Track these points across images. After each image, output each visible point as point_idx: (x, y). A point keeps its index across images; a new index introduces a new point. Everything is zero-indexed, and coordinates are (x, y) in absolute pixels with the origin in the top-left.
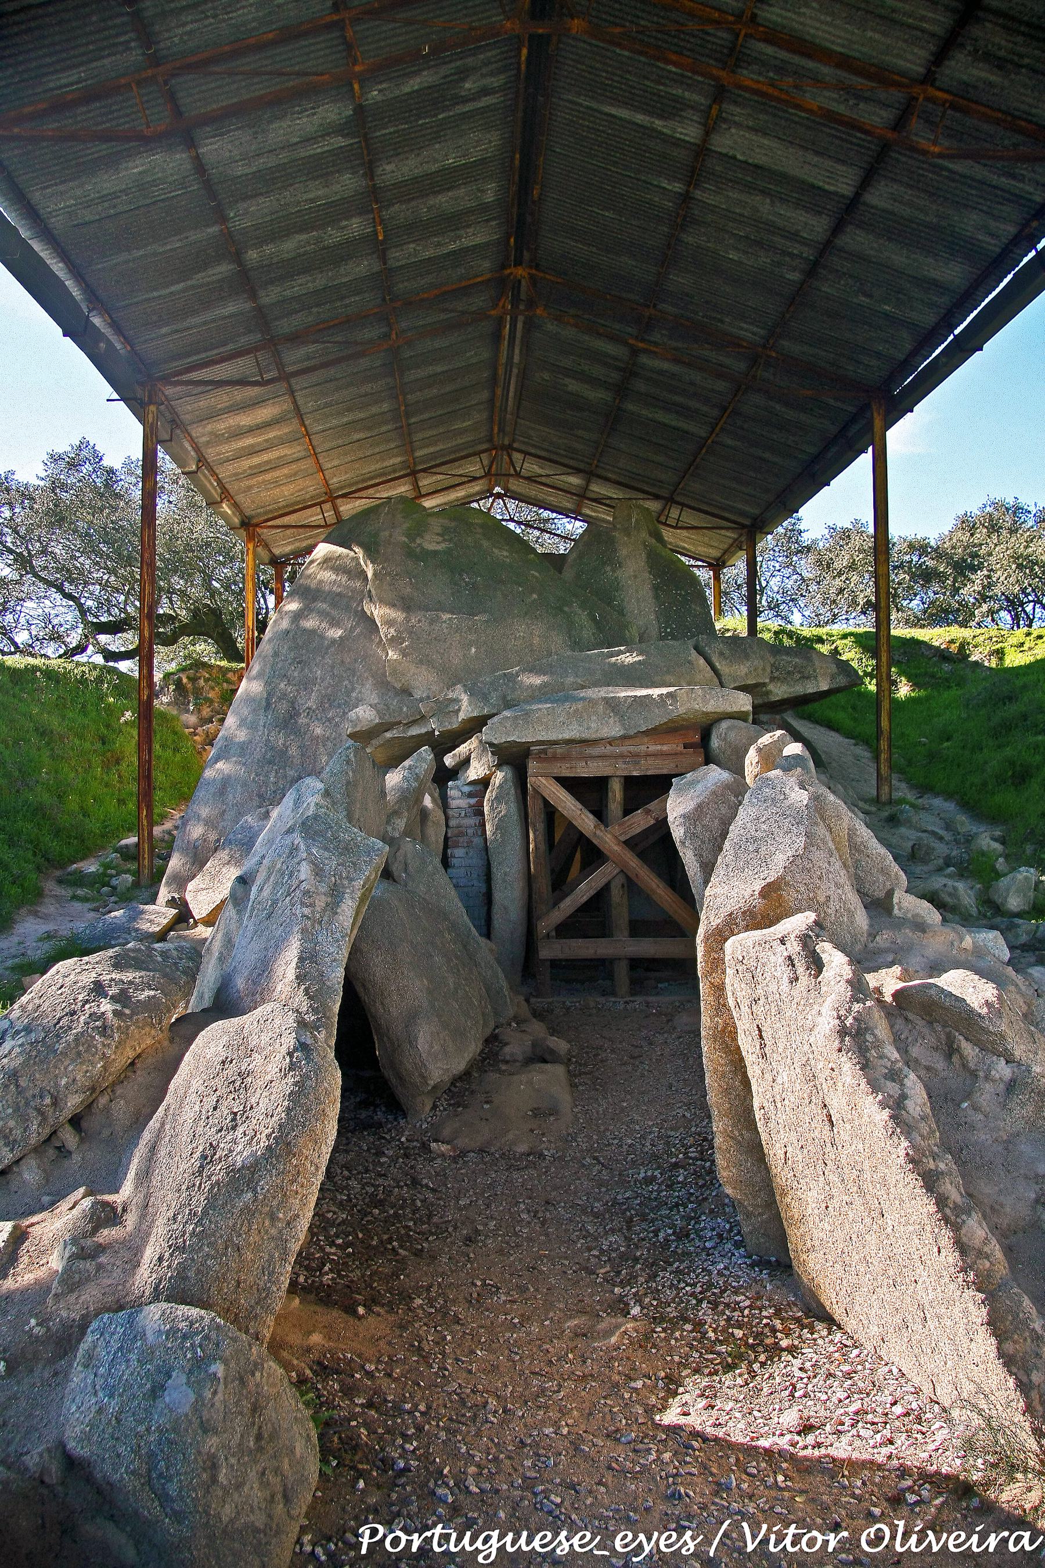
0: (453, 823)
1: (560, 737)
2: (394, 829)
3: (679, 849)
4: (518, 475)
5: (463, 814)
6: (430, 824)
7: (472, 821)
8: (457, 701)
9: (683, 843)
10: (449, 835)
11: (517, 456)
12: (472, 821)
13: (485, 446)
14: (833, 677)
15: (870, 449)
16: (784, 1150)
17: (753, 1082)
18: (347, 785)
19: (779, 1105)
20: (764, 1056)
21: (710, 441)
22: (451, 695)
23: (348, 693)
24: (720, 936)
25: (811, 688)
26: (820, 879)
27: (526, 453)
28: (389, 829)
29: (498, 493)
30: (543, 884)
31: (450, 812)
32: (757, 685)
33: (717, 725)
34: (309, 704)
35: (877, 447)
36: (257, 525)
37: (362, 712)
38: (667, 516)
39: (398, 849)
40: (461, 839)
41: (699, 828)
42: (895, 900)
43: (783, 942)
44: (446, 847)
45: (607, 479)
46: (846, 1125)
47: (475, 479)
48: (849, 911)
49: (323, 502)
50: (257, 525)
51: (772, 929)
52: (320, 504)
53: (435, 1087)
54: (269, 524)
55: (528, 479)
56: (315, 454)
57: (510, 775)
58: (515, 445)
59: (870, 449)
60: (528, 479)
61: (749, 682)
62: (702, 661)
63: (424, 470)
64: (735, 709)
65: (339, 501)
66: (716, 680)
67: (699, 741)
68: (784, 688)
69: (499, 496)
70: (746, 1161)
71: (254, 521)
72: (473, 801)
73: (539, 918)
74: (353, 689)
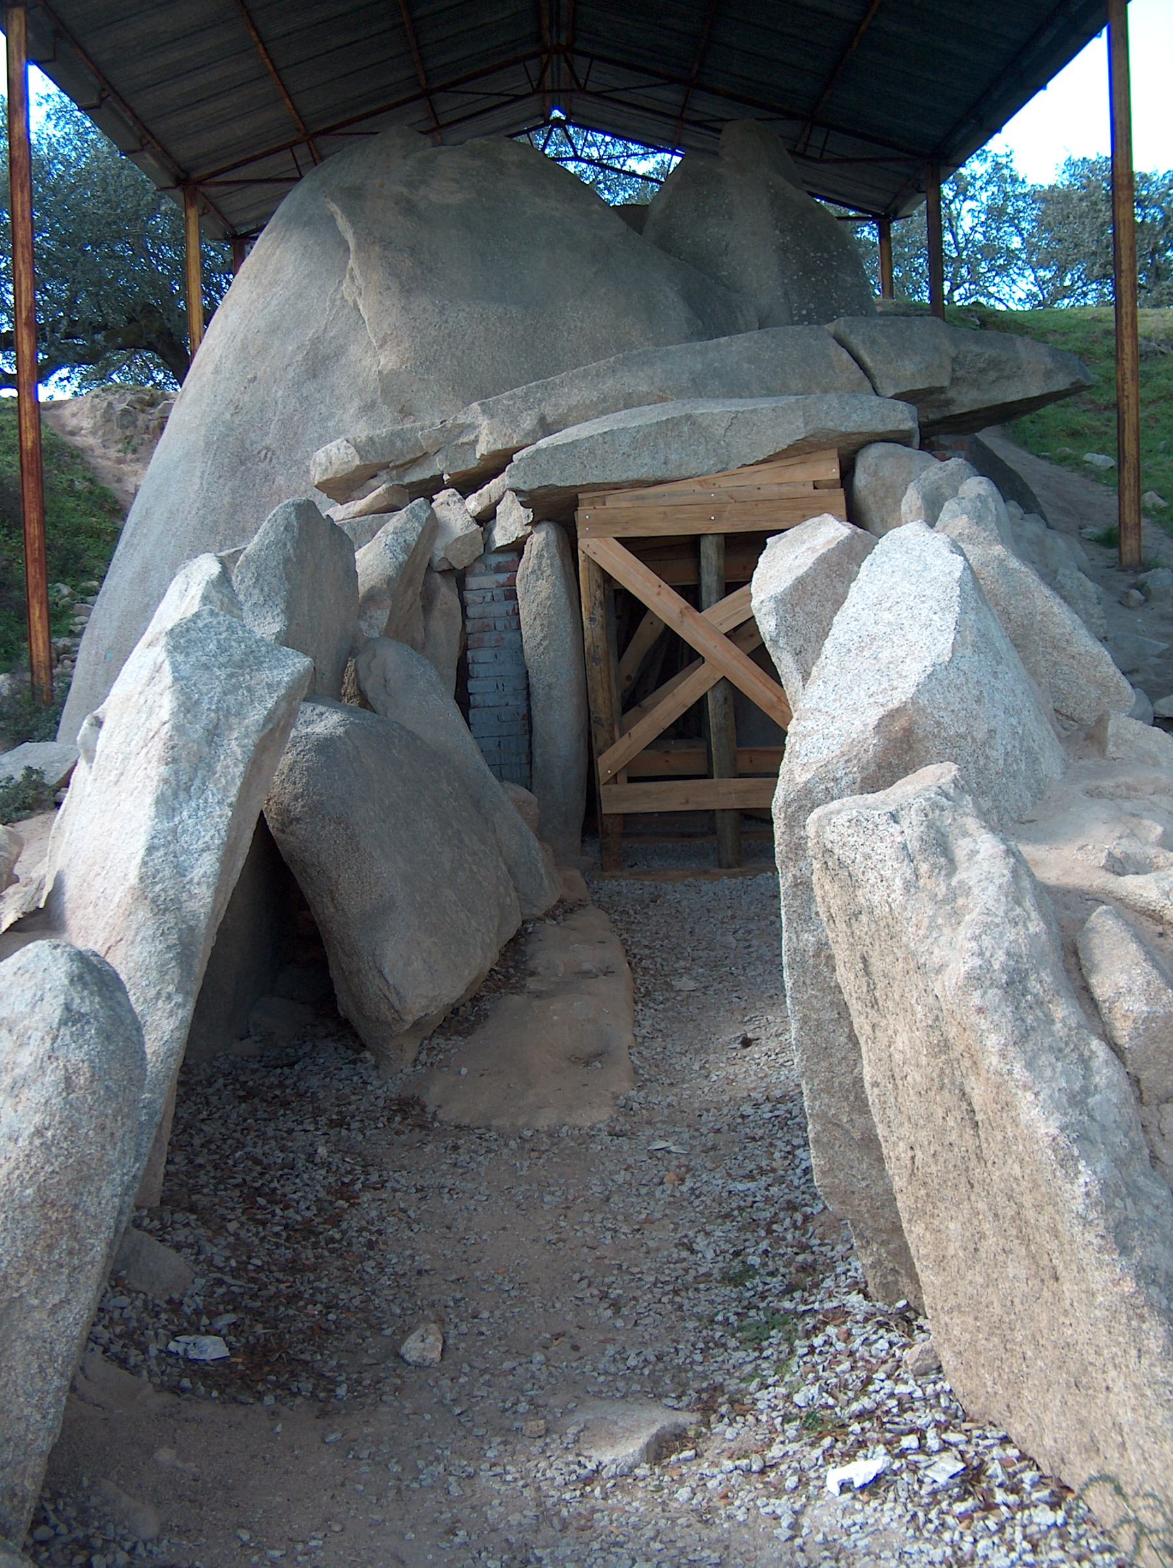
0: (471, 612)
1: (624, 477)
2: (371, 626)
3: (770, 651)
4: (582, 90)
5: (488, 598)
6: (436, 614)
7: (505, 607)
8: (472, 427)
9: (775, 642)
10: (469, 629)
11: (581, 63)
12: (505, 607)
13: (531, 49)
14: (1048, 375)
15: (1105, 31)
16: (910, 1153)
17: (862, 1040)
18: (285, 563)
19: (899, 1083)
20: (874, 1004)
21: (863, 27)
22: (462, 419)
23: (324, 419)
24: (807, 800)
25: (1013, 393)
26: (978, 701)
27: (594, 57)
28: (364, 625)
29: (558, 119)
30: (605, 702)
31: (469, 596)
32: (930, 391)
33: (864, 450)
34: (268, 441)
35: (1113, 28)
36: (200, 182)
37: (335, 450)
38: (806, 145)
39: (375, 656)
40: (486, 636)
41: (801, 618)
42: (1111, 730)
43: (894, 818)
44: (465, 649)
45: (715, 92)
46: (996, 1132)
47: (517, 98)
48: (1029, 752)
49: (295, 143)
50: (200, 182)
51: (881, 795)
52: (290, 146)
53: (416, 1024)
54: (218, 179)
55: (597, 94)
56: (276, 71)
57: (553, 537)
58: (578, 45)
59: (1105, 31)
60: (597, 94)
61: (919, 386)
62: (845, 356)
63: (443, 89)
64: (890, 427)
65: (318, 140)
66: (867, 384)
67: (838, 476)
68: (974, 394)
69: (558, 123)
70: (860, 1161)
71: (195, 175)
72: (503, 578)
73: (600, 753)
74: (331, 415)
